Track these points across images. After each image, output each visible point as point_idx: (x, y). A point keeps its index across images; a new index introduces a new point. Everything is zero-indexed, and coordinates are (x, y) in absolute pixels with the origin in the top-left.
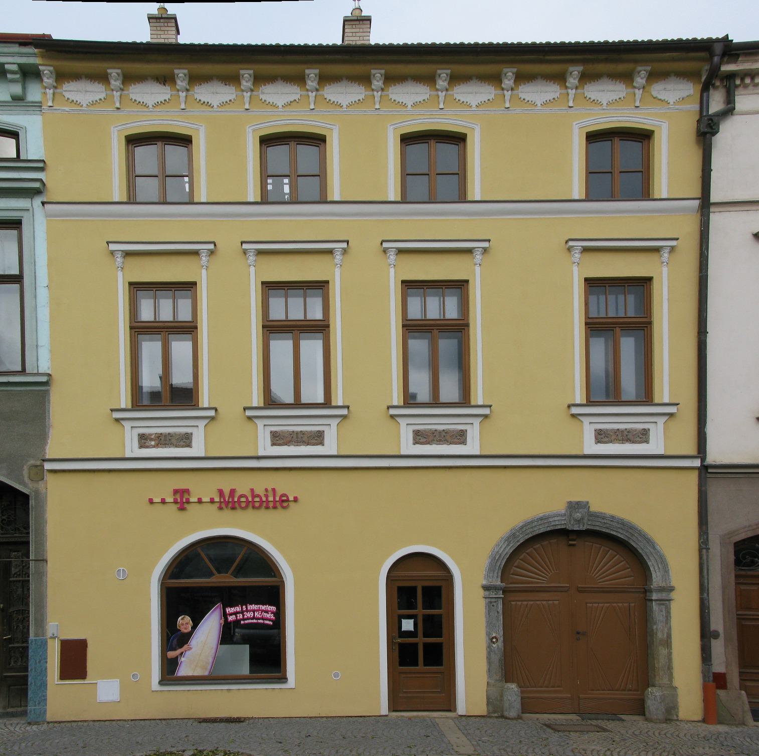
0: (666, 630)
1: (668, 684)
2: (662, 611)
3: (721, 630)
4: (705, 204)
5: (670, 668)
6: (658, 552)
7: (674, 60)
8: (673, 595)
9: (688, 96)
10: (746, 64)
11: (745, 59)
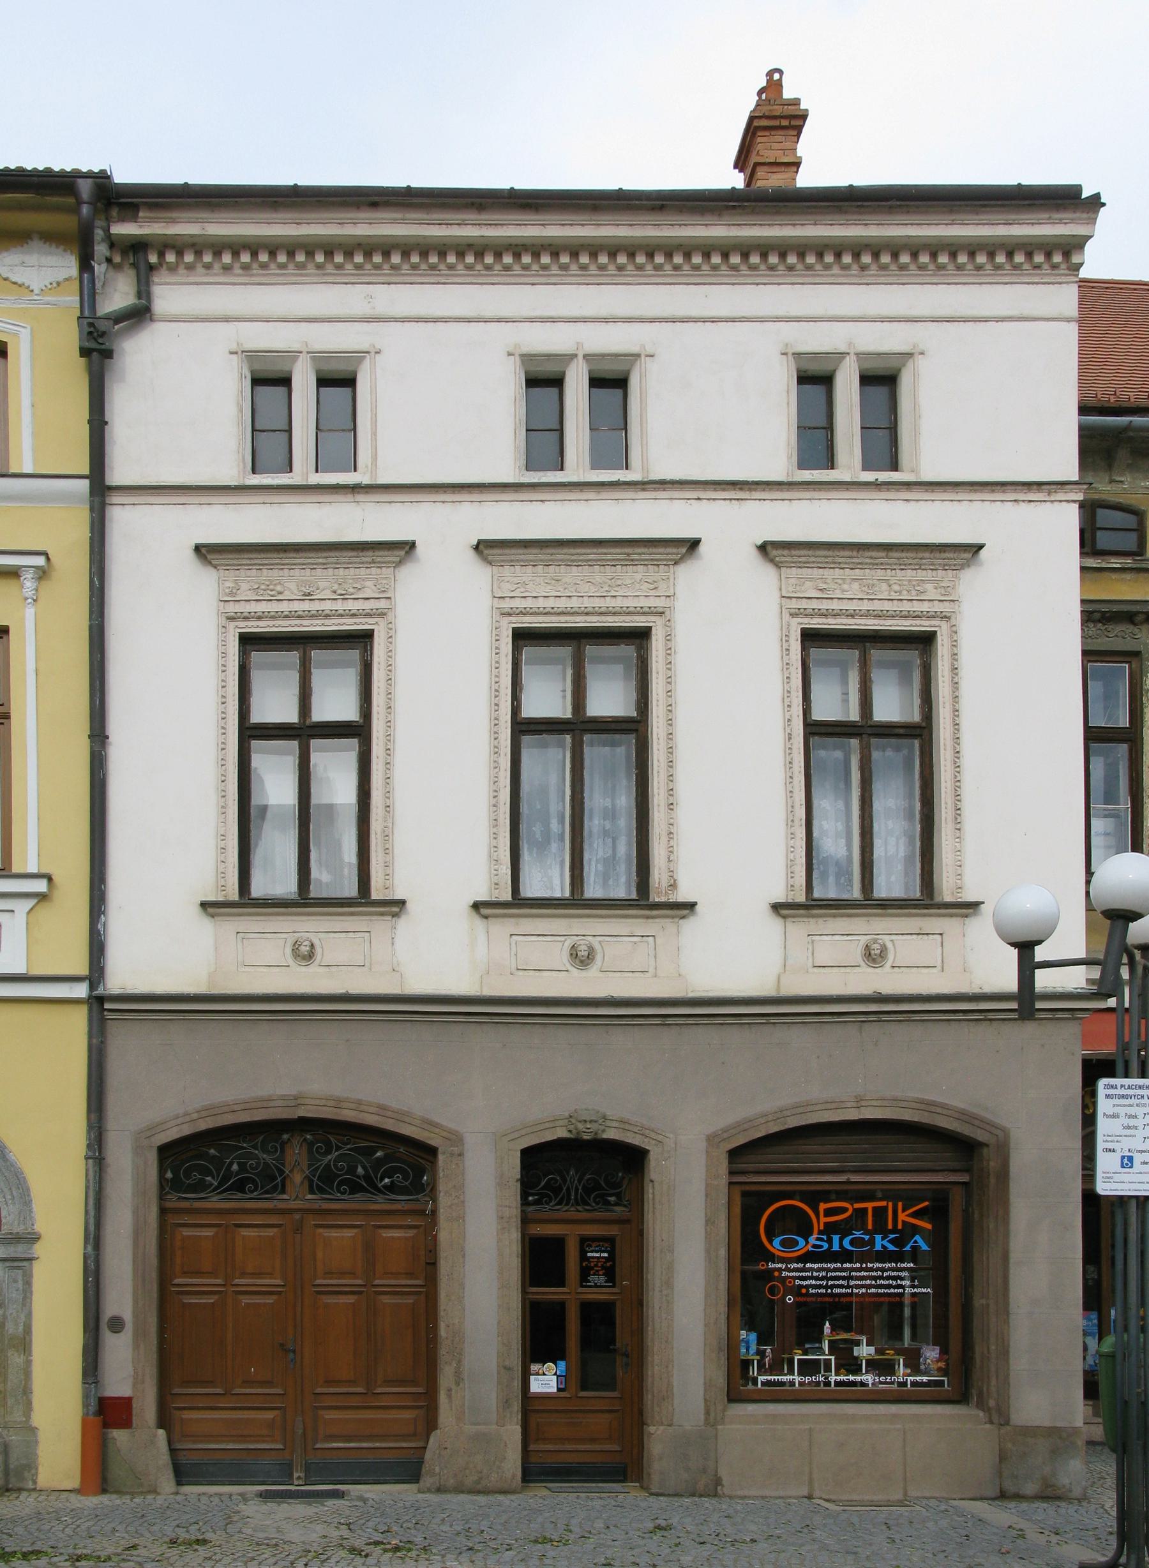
0: (22, 1316)
1: (21, 1422)
2: (15, 1281)
3: (128, 1316)
4: (100, 490)
5: (27, 1391)
6: (12, 1165)
7: (21, 207)
8: (38, 1249)
9: (66, 280)
10: (156, 225)
11: (151, 215)
